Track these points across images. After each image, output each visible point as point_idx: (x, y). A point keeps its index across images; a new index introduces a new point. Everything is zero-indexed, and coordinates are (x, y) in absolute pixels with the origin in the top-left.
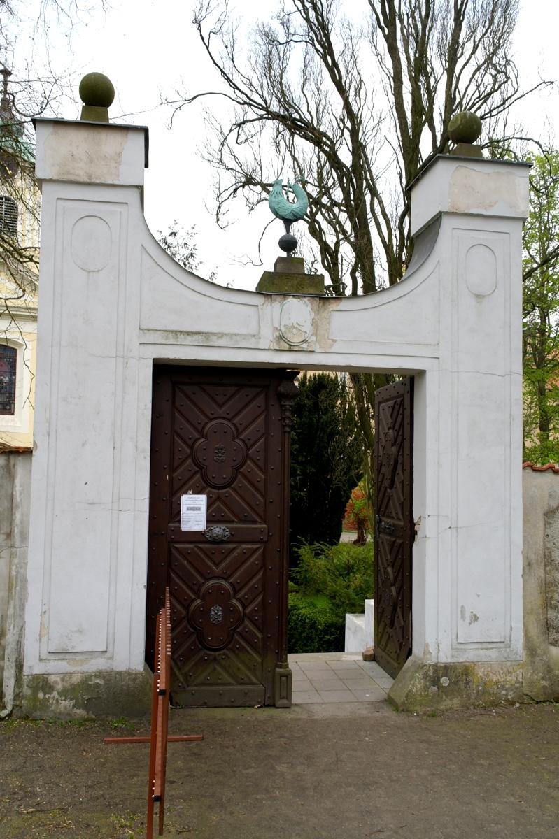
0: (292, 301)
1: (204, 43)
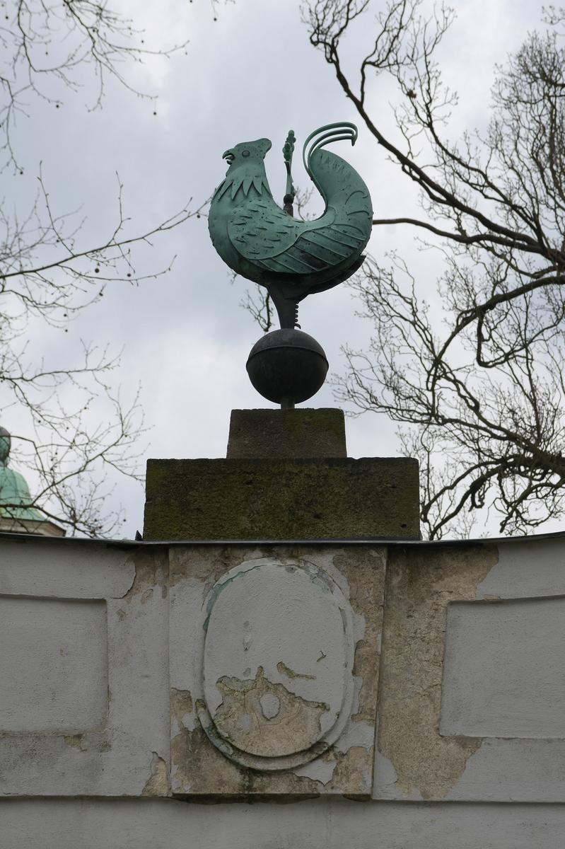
0: (261, 574)
1: (350, 95)
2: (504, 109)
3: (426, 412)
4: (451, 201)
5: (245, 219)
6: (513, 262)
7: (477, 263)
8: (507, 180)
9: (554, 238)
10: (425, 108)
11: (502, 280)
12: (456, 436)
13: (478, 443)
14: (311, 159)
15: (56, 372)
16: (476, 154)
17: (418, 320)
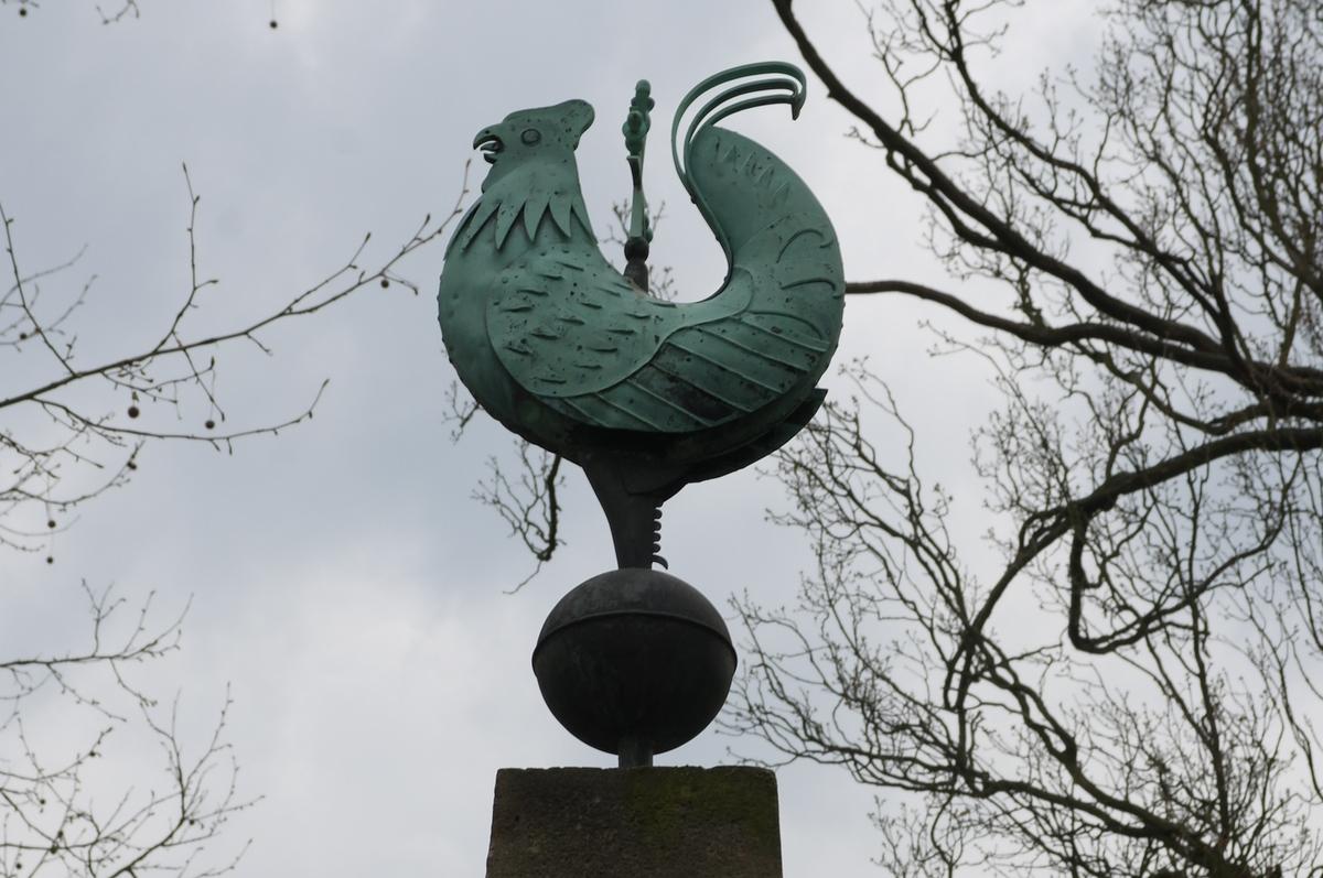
2: (1134, 18)
3: (944, 762)
4: (1008, 241)
5: (531, 296)
6: (1158, 392)
7: (1071, 392)
8: (1145, 192)
9: (1259, 334)
10: (943, 12)
11: (1133, 437)
12: (1020, 825)
13: (1072, 841)
14: (692, 149)
15: (19, 663)
16: (1072, 129)
17: (925, 534)
